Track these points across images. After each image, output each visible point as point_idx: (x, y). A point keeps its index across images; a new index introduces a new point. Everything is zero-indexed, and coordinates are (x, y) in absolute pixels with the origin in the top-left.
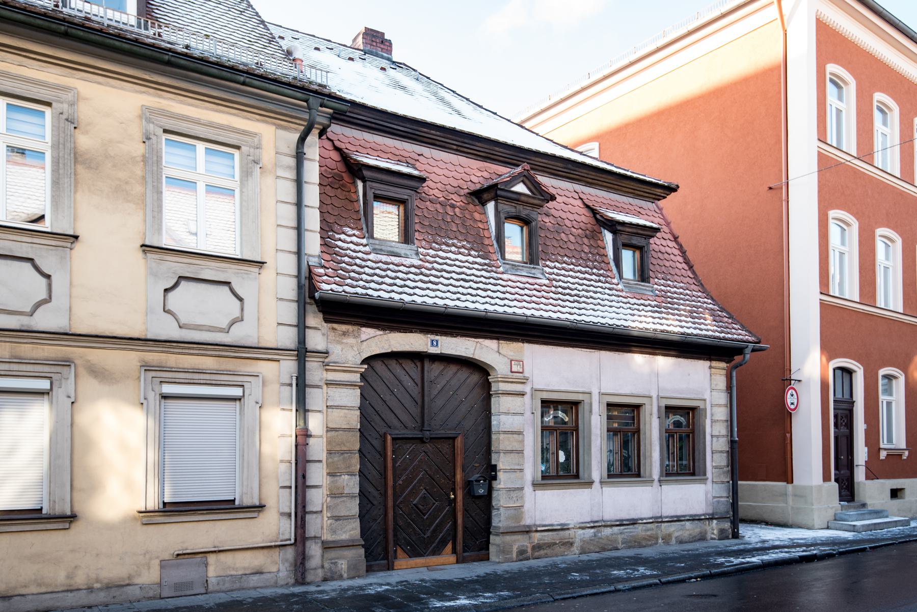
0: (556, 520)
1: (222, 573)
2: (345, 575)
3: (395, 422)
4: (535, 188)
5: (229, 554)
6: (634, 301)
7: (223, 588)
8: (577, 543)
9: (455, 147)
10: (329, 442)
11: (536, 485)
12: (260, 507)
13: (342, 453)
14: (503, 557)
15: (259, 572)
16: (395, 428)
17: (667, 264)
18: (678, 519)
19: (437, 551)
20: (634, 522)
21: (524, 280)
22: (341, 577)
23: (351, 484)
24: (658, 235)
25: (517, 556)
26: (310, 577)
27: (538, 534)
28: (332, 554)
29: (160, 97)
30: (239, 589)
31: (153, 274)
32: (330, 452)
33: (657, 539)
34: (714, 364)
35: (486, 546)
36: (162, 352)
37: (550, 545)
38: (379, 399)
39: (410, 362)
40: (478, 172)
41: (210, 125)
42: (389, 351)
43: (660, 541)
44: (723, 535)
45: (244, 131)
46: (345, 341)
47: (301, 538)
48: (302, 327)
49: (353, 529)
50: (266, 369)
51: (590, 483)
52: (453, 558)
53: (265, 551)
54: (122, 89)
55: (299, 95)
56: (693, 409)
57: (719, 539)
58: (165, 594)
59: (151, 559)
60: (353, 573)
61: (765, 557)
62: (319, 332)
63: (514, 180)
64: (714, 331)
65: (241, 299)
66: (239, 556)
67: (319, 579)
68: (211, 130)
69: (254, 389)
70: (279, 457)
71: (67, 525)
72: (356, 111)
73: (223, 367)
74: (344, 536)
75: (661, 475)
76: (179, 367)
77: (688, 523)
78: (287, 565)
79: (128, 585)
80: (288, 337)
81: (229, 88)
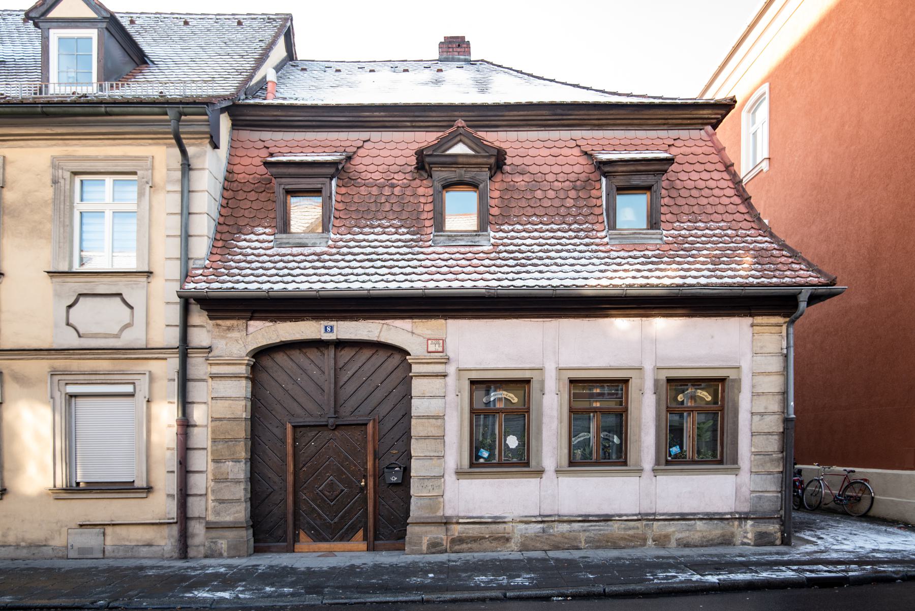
0: (487, 511)
1: (117, 543)
2: (225, 554)
3: (299, 411)
4: (477, 145)
5: (124, 528)
6: (622, 254)
7: (118, 555)
8: (516, 539)
9: (409, 124)
10: (213, 432)
11: (460, 474)
12: (149, 489)
13: (226, 441)
14: (420, 546)
15: (150, 545)
16: (298, 416)
17: (704, 201)
18: (683, 517)
19: (346, 536)
20: (606, 519)
21: (463, 250)
22: (220, 555)
23: (236, 470)
24: (674, 167)
25: (428, 548)
26: (192, 552)
27: (459, 527)
28: (214, 534)
29: (67, 145)
30: (131, 558)
31: (58, 295)
32: (214, 441)
33: (645, 540)
34: (759, 320)
35: (402, 535)
36: (66, 359)
37: (475, 539)
38: (280, 389)
39: (316, 350)
40: (410, 142)
41: (107, 159)
42: (278, 341)
43: (650, 542)
44: (762, 539)
45: (136, 157)
46: (229, 335)
47: (184, 518)
48: (185, 326)
49: (237, 512)
50: (156, 367)
51: (540, 473)
52: (363, 546)
53: (155, 527)
54: (38, 147)
55: (156, 110)
56: (723, 380)
57: (756, 545)
58: (72, 554)
59: (62, 527)
60: (233, 553)
61: (732, 576)
62: (204, 329)
63: (445, 143)
64: (747, 277)
65: (131, 308)
66: (133, 529)
67: (201, 555)
68: (111, 163)
69: (143, 385)
70: (166, 446)
71: (144, 495)
72: (291, 113)
73: (117, 368)
74: (228, 519)
75: (657, 462)
76: (78, 369)
77: (698, 523)
78: (173, 540)
79: (45, 546)
80: (172, 337)
81: (89, 122)
